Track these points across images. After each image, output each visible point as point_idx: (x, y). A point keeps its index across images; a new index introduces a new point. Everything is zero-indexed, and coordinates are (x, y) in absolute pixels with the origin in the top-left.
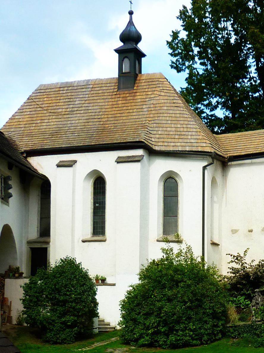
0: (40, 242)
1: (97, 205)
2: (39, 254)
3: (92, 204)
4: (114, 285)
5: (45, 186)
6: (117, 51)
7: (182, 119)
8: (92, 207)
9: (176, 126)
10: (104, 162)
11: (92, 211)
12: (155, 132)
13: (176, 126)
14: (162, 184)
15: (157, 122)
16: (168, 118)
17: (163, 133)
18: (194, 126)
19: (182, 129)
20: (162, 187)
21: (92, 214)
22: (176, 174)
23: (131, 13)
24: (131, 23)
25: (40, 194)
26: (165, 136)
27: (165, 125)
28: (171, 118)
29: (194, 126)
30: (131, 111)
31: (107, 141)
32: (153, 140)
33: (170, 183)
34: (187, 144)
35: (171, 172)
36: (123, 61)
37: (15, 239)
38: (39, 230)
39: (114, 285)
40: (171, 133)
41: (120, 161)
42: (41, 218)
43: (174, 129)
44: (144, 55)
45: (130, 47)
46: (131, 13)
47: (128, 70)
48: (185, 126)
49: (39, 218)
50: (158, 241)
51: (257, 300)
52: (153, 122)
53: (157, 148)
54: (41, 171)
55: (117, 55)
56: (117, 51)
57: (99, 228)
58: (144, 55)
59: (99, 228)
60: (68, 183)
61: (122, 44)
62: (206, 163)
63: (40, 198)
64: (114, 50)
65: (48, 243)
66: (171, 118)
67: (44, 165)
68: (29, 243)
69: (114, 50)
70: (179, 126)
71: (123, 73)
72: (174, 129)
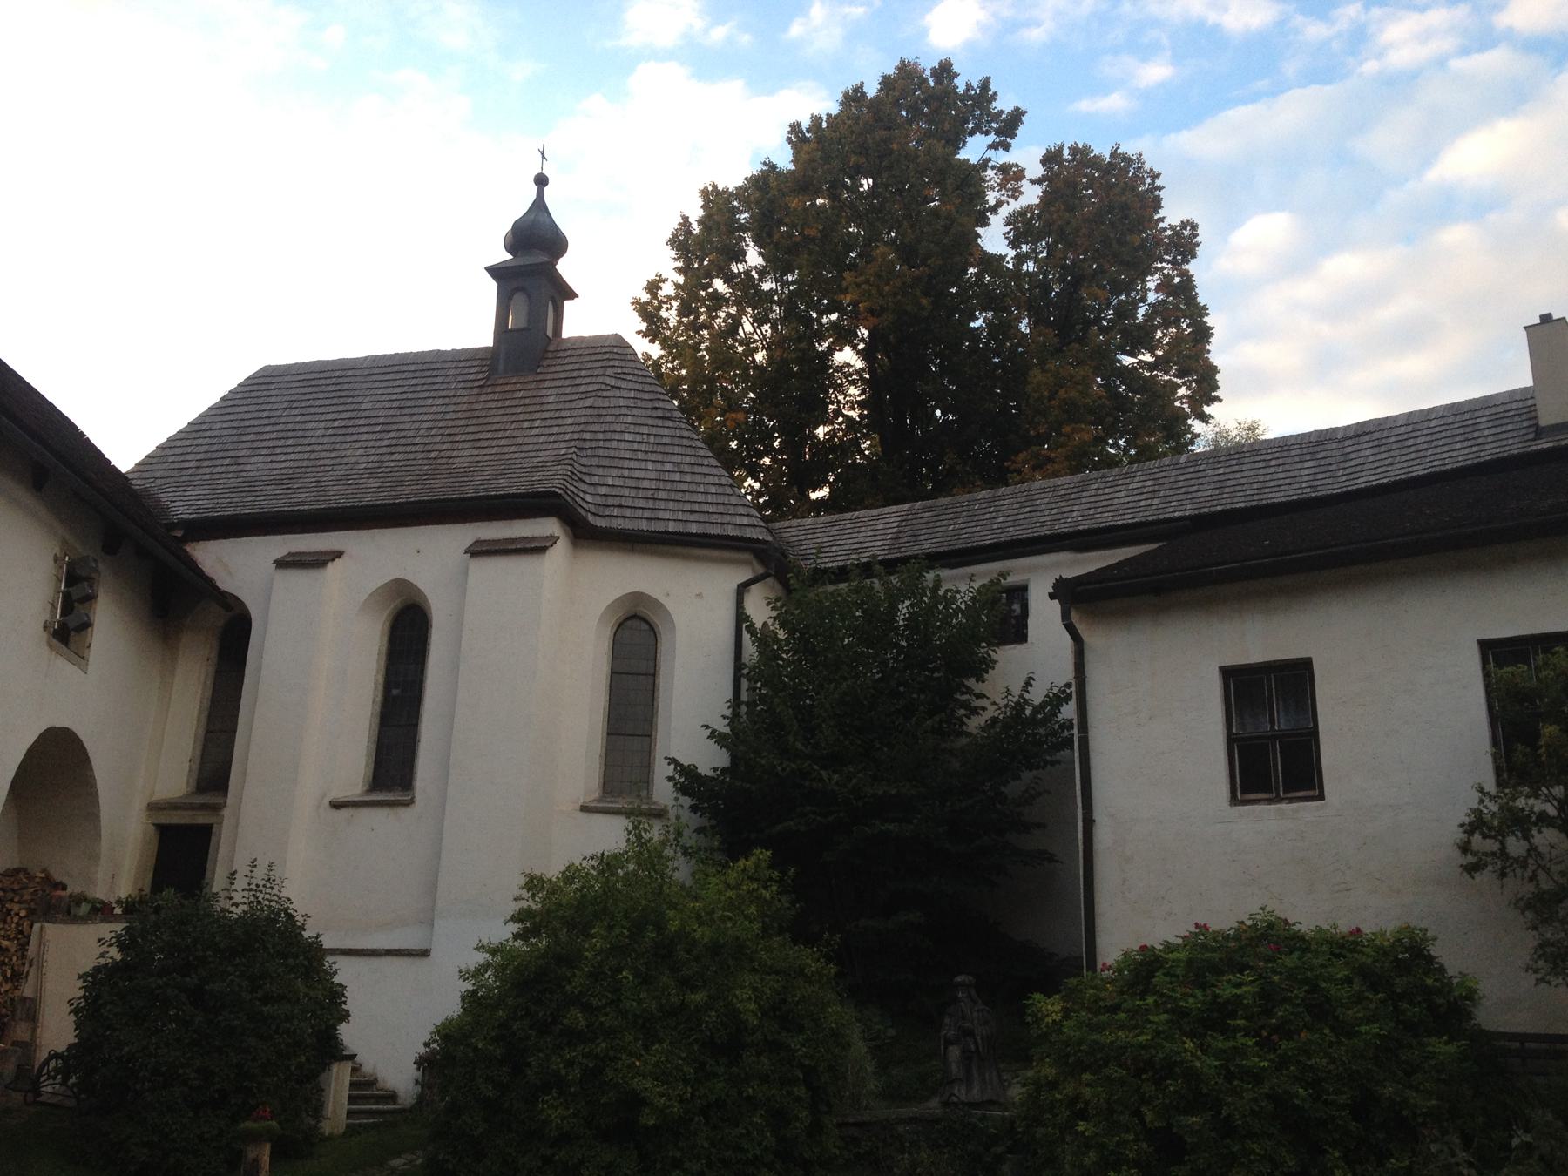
0: (192, 807)
1: (395, 692)
2: (183, 847)
3: (380, 688)
4: (425, 953)
5: (233, 635)
6: (494, 271)
7: (676, 450)
8: (379, 699)
9: (659, 466)
10: (428, 558)
11: (378, 708)
12: (596, 480)
13: (659, 466)
14: (608, 633)
15: (601, 452)
16: (636, 446)
17: (617, 482)
18: (715, 471)
19: (677, 477)
20: (605, 646)
21: (377, 720)
22: (657, 605)
23: (541, 181)
24: (539, 205)
25: (214, 655)
26: (626, 492)
27: (626, 464)
28: (643, 447)
29: (715, 471)
30: (526, 425)
31: (440, 489)
32: (588, 498)
33: (636, 636)
34: (692, 517)
35: (638, 597)
36: (510, 298)
37: (100, 785)
38: (196, 767)
39: (425, 953)
40: (646, 484)
41: (479, 551)
42: (208, 732)
43: (653, 475)
44: (572, 295)
45: (532, 263)
46: (541, 181)
47: (522, 324)
48: (686, 468)
49: (201, 732)
50: (585, 809)
51: (963, 1018)
52: (589, 452)
53: (600, 523)
54: (225, 583)
55: (492, 287)
56: (494, 271)
57: (393, 767)
58: (572, 295)
59: (393, 767)
60: (314, 628)
61: (510, 257)
62: (744, 575)
63: (212, 670)
64: (488, 269)
65: (216, 809)
66: (643, 447)
67: (238, 566)
68: (154, 807)
69: (488, 269)
70: (668, 467)
71: (507, 331)
72: (653, 475)
